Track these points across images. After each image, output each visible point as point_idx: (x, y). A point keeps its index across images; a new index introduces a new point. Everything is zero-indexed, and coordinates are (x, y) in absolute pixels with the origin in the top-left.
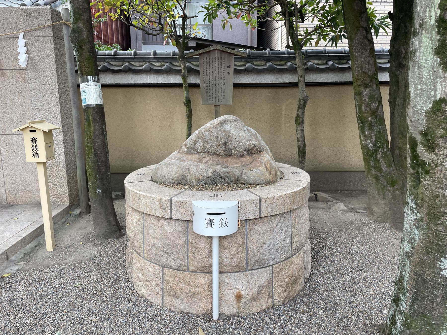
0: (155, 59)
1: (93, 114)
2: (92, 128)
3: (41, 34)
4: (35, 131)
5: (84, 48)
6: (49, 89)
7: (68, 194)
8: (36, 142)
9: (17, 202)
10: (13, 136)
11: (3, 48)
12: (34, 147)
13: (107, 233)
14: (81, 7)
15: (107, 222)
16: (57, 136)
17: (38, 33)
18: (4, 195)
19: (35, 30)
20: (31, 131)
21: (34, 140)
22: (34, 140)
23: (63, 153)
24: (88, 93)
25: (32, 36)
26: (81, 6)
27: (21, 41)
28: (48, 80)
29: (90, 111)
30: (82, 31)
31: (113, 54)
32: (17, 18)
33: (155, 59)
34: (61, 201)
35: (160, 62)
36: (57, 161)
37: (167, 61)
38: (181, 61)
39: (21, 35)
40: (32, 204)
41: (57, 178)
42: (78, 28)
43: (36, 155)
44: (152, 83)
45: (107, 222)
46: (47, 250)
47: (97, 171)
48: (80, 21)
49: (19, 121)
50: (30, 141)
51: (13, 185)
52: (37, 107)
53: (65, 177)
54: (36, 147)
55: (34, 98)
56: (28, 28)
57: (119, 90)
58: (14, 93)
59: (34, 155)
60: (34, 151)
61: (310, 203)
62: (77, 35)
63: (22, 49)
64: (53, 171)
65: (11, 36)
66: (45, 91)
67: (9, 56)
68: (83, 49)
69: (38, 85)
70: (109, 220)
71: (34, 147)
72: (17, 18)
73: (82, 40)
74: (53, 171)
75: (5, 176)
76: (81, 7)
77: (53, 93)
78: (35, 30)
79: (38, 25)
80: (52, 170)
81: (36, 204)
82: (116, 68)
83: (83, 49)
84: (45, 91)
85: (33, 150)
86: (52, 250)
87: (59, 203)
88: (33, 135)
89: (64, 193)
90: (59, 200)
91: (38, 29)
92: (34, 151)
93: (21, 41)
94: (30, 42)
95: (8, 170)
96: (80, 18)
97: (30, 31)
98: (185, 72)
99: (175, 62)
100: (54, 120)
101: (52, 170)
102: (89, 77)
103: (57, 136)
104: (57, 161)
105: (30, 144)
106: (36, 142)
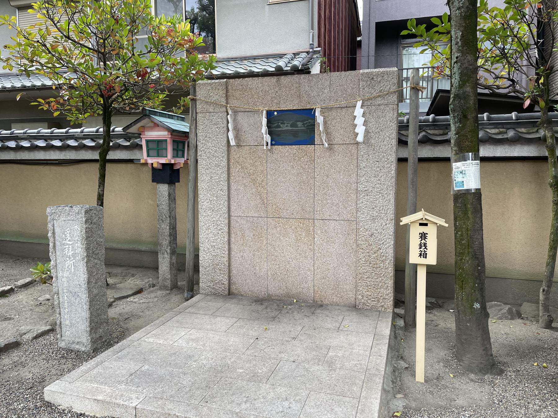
0: (490, 124)
1: (473, 202)
2: (471, 220)
3: (383, 101)
4: (426, 225)
5: (469, 117)
6: (383, 167)
7: (392, 299)
8: (425, 238)
9: (326, 302)
10: (331, 221)
11: (333, 119)
12: (423, 245)
13: (482, 366)
14: (471, 67)
15: (484, 350)
16: (386, 224)
17: (379, 101)
18: (312, 291)
19: (375, 98)
20: (421, 224)
21: (423, 236)
22: (423, 236)
23: (392, 246)
24: (467, 174)
25: (371, 105)
26: (471, 65)
27: (359, 111)
28: (384, 156)
29: (470, 197)
30: (469, 96)
31: (431, 120)
32: (354, 85)
33: (490, 124)
34: (382, 306)
35: (498, 128)
36: (383, 256)
37: (508, 126)
38: (546, 127)
39: (359, 104)
40: (344, 306)
41: (381, 277)
42: (464, 93)
43: (424, 255)
44: (487, 155)
45: (484, 350)
46: (417, 380)
47: (477, 278)
48: (468, 84)
49: (340, 204)
50: (418, 236)
51: (323, 280)
52: (366, 189)
53: (391, 277)
54: (425, 245)
55: (364, 178)
56: (367, 96)
57: (434, 165)
58: (339, 172)
59: (421, 255)
60: (421, 250)
61: (184, 253)
62: (462, 101)
63: (359, 121)
64: (376, 268)
65: (344, 103)
66: (378, 169)
67: (339, 128)
68: (468, 119)
69: (371, 162)
70: (486, 348)
71: (423, 245)
72: (354, 85)
73: (468, 108)
74: (376, 268)
75: (315, 268)
76: (471, 67)
77: (389, 172)
78: (375, 98)
79: (380, 91)
80: (376, 266)
81: (349, 307)
82: (439, 138)
83: (468, 119)
84: (378, 169)
85: (420, 248)
86: (423, 381)
87: (380, 309)
88: (423, 229)
89: (387, 297)
90: (379, 305)
91: (379, 96)
92: (421, 250)
93: (359, 111)
94: (368, 111)
95: (320, 261)
96: (468, 81)
97: (369, 99)
98: (553, 141)
99: (521, 128)
100: (385, 204)
101: (376, 266)
102: (470, 154)
103: (386, 224)
104: (383, 256)
105: (418, 241)
106: (425, 238)
